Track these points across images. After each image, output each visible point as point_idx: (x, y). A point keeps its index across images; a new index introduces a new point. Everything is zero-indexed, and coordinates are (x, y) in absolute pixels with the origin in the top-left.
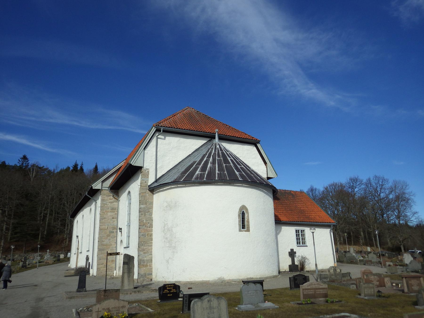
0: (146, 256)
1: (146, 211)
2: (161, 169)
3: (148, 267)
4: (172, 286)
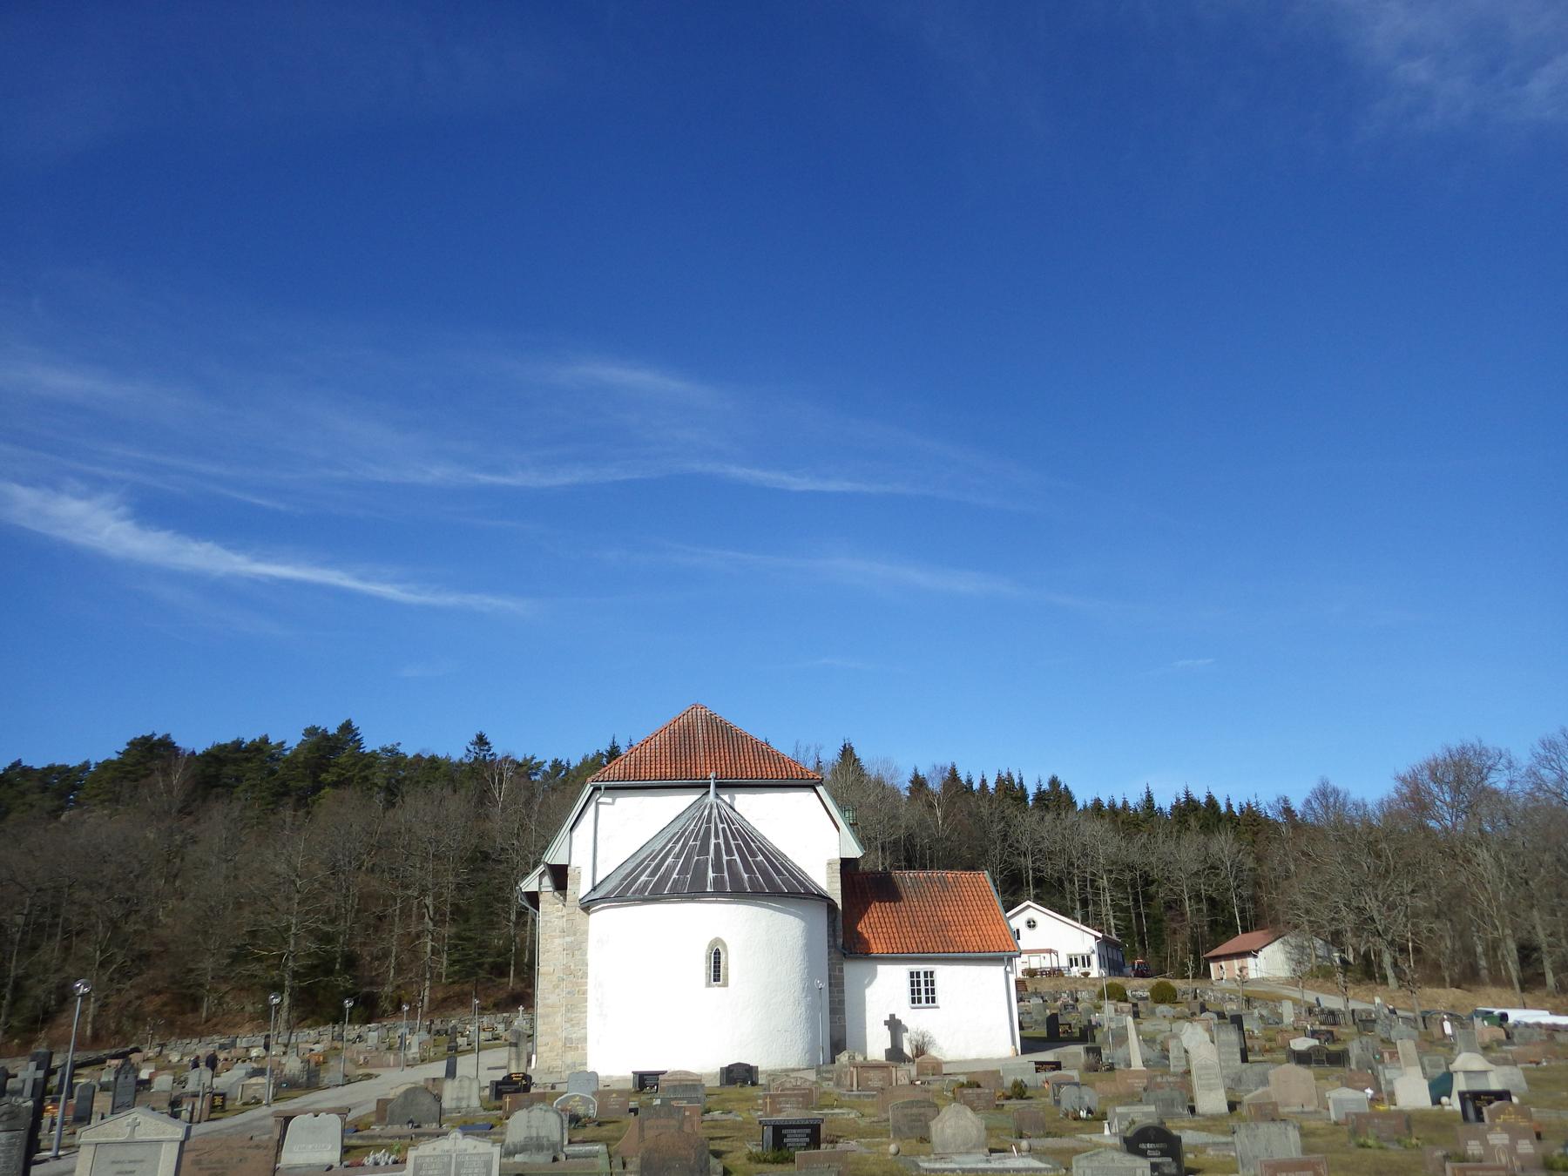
3: (580, 1051)
4: (521, 1075)
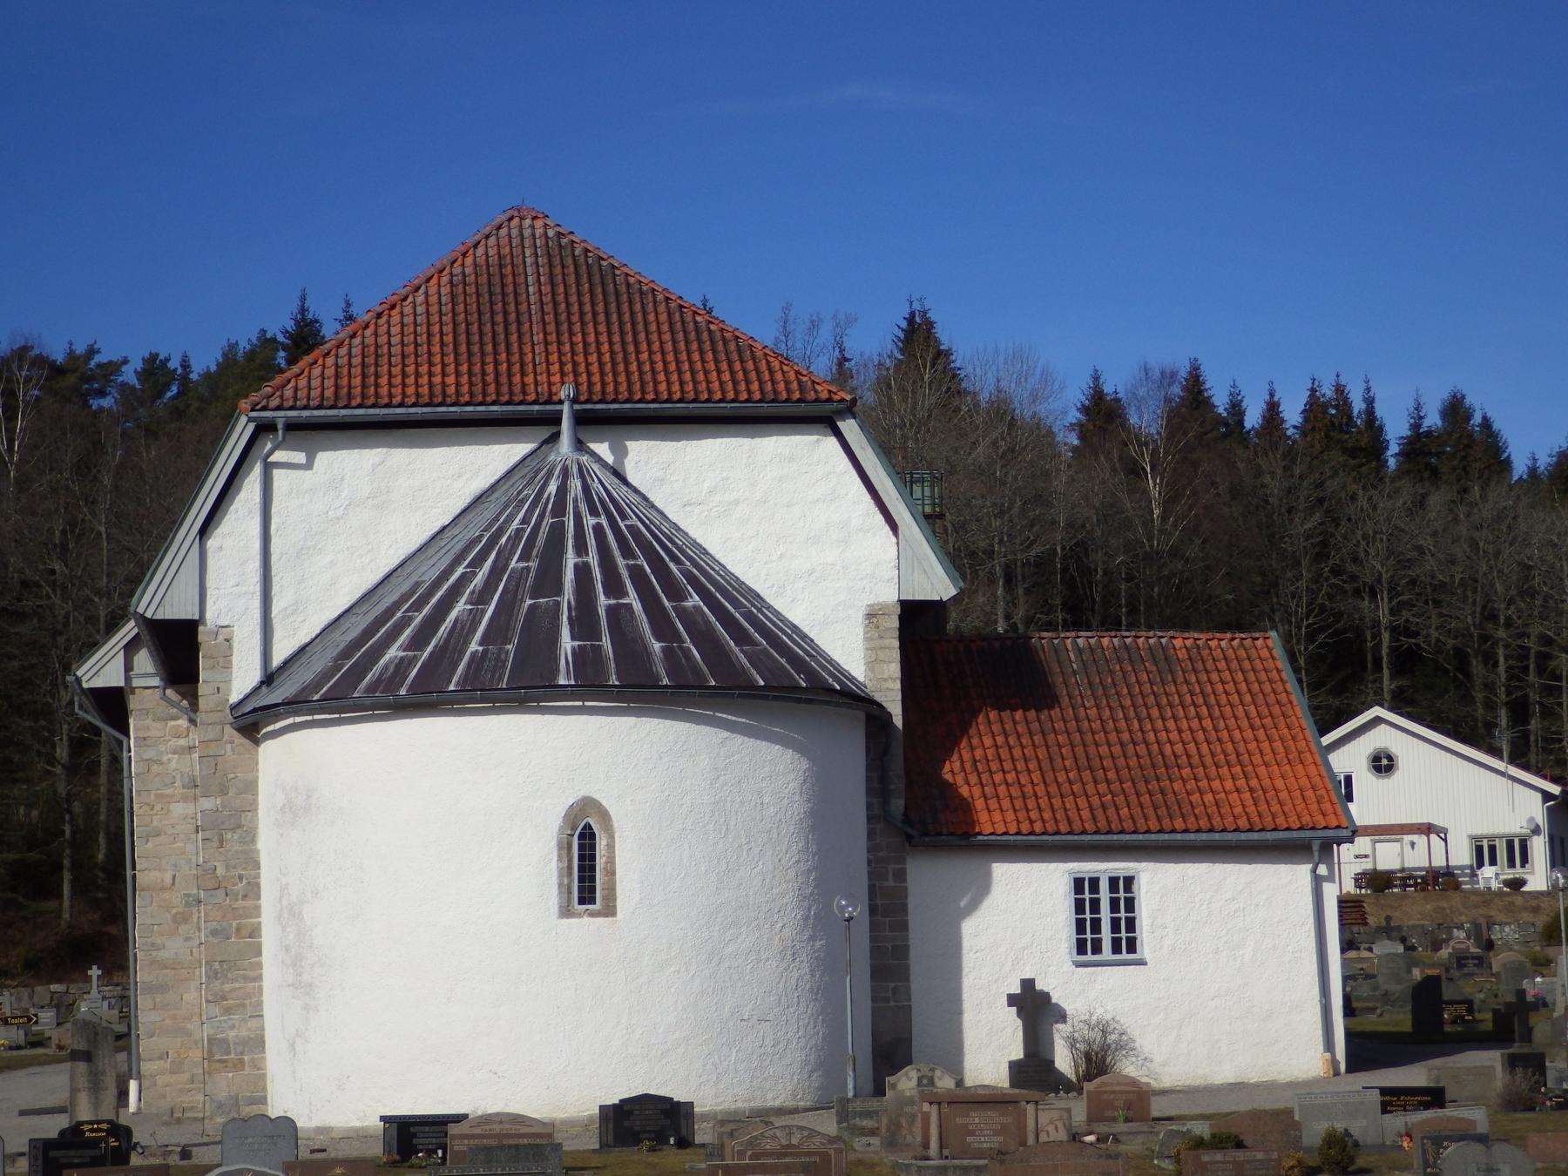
0: (237, 1023)
1: (223, 823)
2: (292, 619)
3: (247, 1070)
4: (105, 1126)
